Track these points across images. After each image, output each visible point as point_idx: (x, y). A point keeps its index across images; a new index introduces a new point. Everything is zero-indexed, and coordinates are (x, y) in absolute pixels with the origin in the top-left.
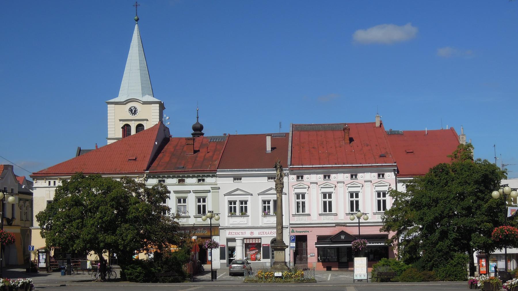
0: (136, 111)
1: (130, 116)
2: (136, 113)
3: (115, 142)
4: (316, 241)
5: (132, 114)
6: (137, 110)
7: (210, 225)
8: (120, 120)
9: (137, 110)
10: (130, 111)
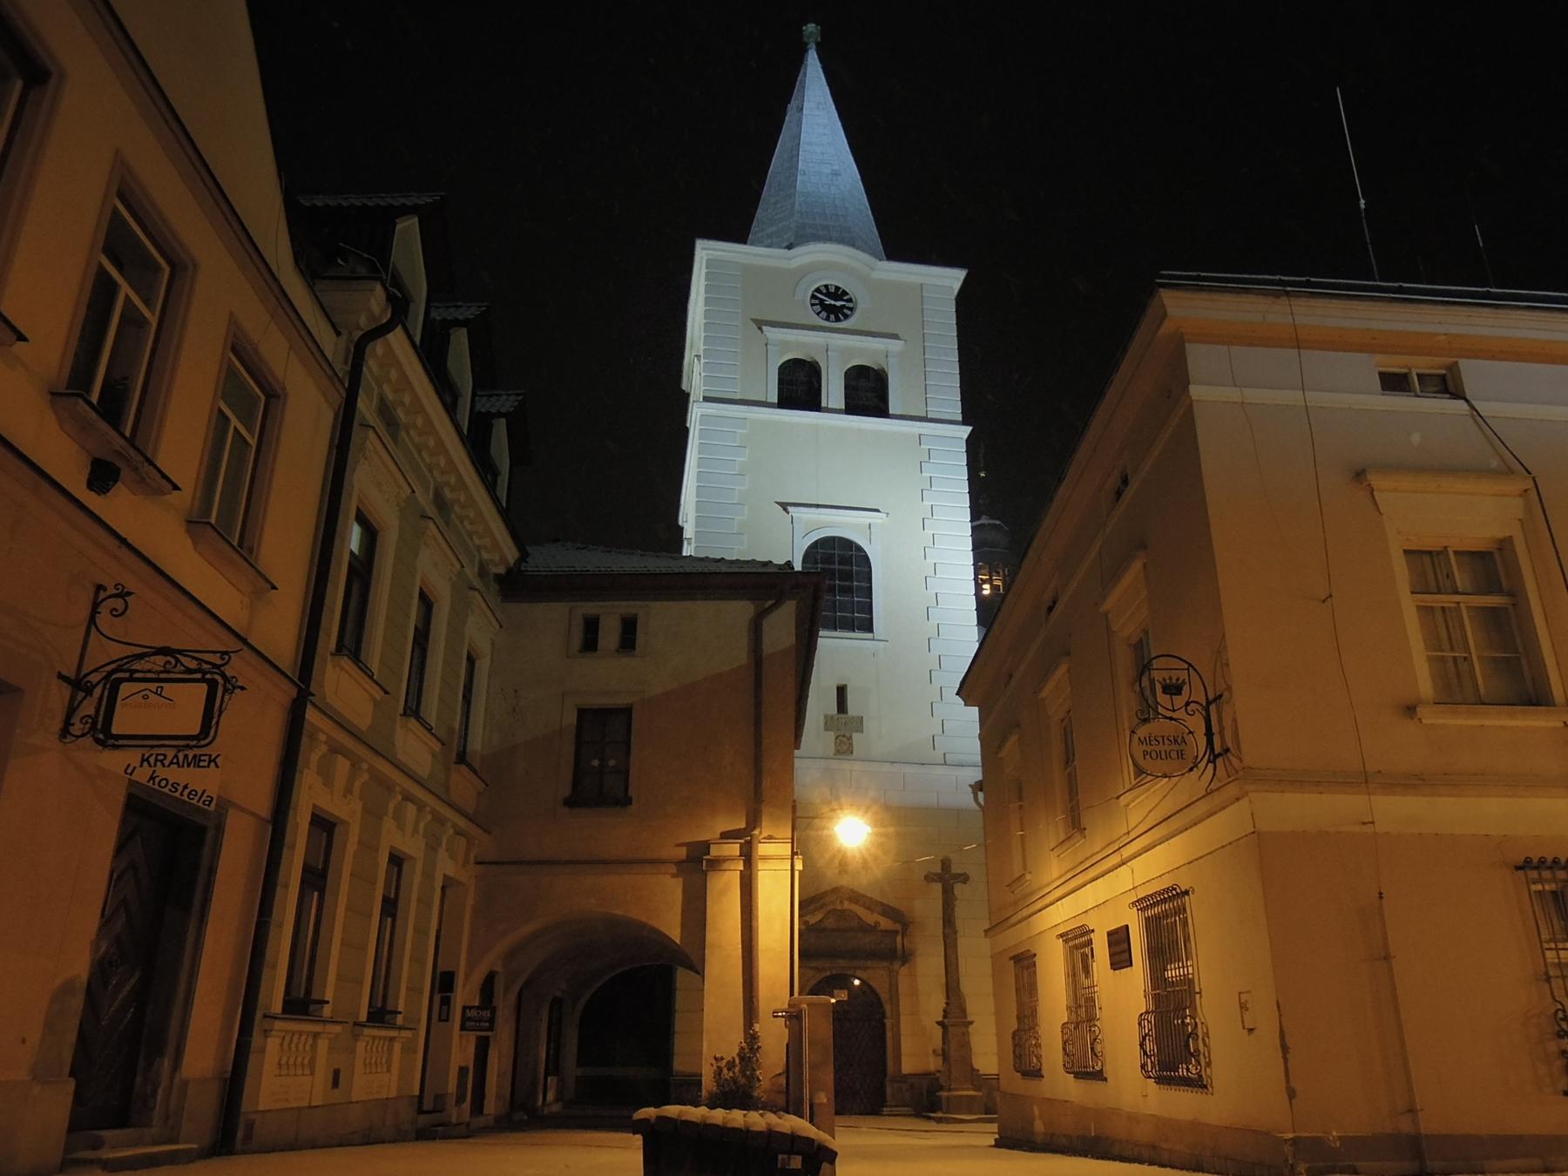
2: (846, 311)
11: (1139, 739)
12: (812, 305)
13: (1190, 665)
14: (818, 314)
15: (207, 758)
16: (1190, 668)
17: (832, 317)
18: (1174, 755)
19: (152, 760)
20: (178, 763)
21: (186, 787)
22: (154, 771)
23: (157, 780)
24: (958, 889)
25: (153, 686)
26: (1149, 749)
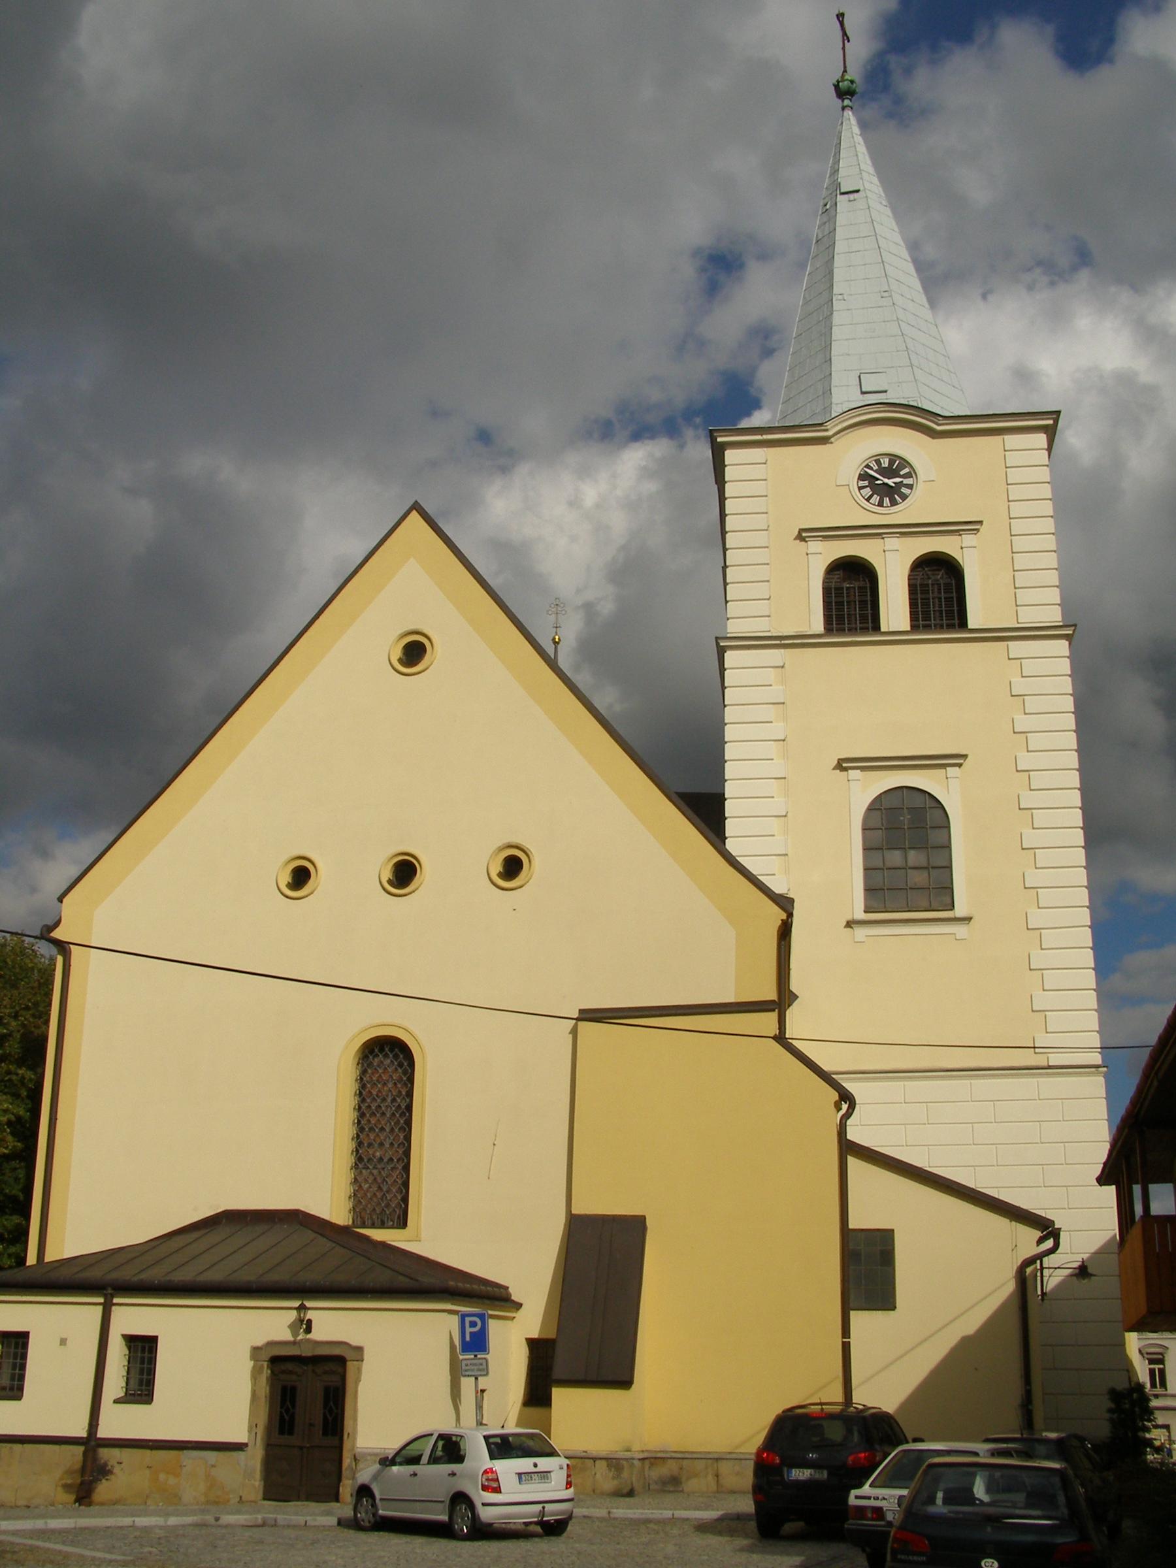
2: (904, 490)
10: (866, 483)
12: (860, 488)
14: (868, 500)
17: (887, 501)
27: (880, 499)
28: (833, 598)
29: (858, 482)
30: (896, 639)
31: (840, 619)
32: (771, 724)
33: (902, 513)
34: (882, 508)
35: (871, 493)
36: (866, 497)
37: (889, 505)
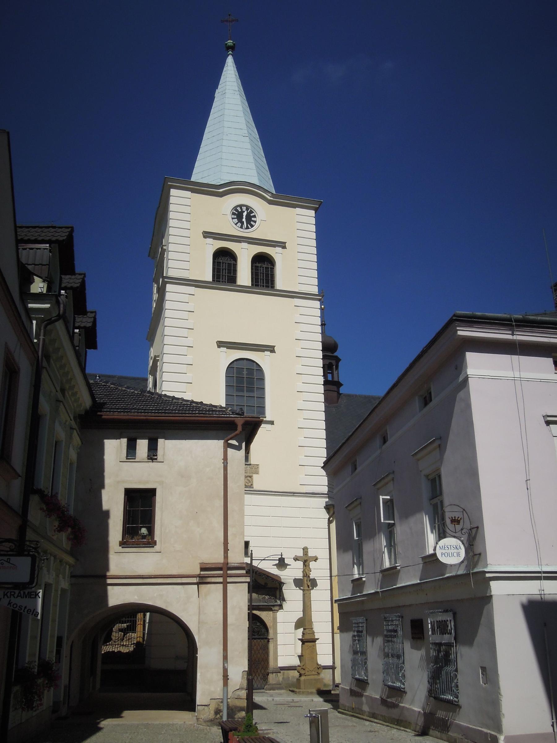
0: (253, 219)
1: (232, 228)
2: (252, 223)
3: (336, 521)
4: (120, 539)
5: (456, 518)
6: (255, 216)
7: (229, 580)
8: (207, 235)
9: (255, 216)
10: (235, 217)
11: (440, 547)
12: (233, 218)
13: (464, 510)
14: (236, 224)
15: (34, 593)
16: (464, 511)
18: (455, 554)
19: (9, 594)
20: (21, 596)
21: (25, 607)
22: (10, 600)
23: (12, 604)
24: (312, 564)
25: (5, 558)
26: (444, 551)
27: (241, 225)
28: (216, 266)
29: (255, 225)
30: (243, 289)
31: (218, 277)
32: (187, 321)
33: (253, 233)
34: (235, 226)
35: (237, 221)
36: (235, 223)
37: (240, 227)
